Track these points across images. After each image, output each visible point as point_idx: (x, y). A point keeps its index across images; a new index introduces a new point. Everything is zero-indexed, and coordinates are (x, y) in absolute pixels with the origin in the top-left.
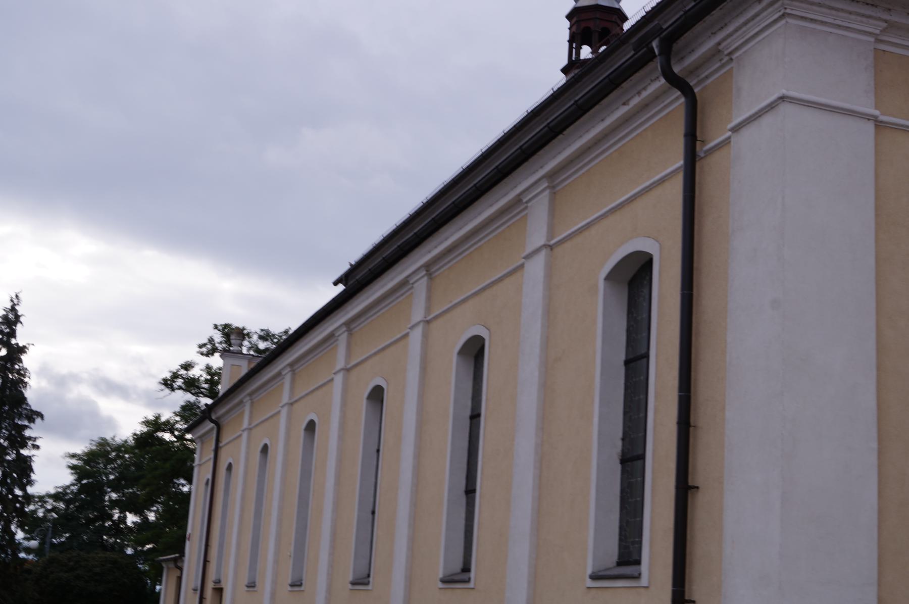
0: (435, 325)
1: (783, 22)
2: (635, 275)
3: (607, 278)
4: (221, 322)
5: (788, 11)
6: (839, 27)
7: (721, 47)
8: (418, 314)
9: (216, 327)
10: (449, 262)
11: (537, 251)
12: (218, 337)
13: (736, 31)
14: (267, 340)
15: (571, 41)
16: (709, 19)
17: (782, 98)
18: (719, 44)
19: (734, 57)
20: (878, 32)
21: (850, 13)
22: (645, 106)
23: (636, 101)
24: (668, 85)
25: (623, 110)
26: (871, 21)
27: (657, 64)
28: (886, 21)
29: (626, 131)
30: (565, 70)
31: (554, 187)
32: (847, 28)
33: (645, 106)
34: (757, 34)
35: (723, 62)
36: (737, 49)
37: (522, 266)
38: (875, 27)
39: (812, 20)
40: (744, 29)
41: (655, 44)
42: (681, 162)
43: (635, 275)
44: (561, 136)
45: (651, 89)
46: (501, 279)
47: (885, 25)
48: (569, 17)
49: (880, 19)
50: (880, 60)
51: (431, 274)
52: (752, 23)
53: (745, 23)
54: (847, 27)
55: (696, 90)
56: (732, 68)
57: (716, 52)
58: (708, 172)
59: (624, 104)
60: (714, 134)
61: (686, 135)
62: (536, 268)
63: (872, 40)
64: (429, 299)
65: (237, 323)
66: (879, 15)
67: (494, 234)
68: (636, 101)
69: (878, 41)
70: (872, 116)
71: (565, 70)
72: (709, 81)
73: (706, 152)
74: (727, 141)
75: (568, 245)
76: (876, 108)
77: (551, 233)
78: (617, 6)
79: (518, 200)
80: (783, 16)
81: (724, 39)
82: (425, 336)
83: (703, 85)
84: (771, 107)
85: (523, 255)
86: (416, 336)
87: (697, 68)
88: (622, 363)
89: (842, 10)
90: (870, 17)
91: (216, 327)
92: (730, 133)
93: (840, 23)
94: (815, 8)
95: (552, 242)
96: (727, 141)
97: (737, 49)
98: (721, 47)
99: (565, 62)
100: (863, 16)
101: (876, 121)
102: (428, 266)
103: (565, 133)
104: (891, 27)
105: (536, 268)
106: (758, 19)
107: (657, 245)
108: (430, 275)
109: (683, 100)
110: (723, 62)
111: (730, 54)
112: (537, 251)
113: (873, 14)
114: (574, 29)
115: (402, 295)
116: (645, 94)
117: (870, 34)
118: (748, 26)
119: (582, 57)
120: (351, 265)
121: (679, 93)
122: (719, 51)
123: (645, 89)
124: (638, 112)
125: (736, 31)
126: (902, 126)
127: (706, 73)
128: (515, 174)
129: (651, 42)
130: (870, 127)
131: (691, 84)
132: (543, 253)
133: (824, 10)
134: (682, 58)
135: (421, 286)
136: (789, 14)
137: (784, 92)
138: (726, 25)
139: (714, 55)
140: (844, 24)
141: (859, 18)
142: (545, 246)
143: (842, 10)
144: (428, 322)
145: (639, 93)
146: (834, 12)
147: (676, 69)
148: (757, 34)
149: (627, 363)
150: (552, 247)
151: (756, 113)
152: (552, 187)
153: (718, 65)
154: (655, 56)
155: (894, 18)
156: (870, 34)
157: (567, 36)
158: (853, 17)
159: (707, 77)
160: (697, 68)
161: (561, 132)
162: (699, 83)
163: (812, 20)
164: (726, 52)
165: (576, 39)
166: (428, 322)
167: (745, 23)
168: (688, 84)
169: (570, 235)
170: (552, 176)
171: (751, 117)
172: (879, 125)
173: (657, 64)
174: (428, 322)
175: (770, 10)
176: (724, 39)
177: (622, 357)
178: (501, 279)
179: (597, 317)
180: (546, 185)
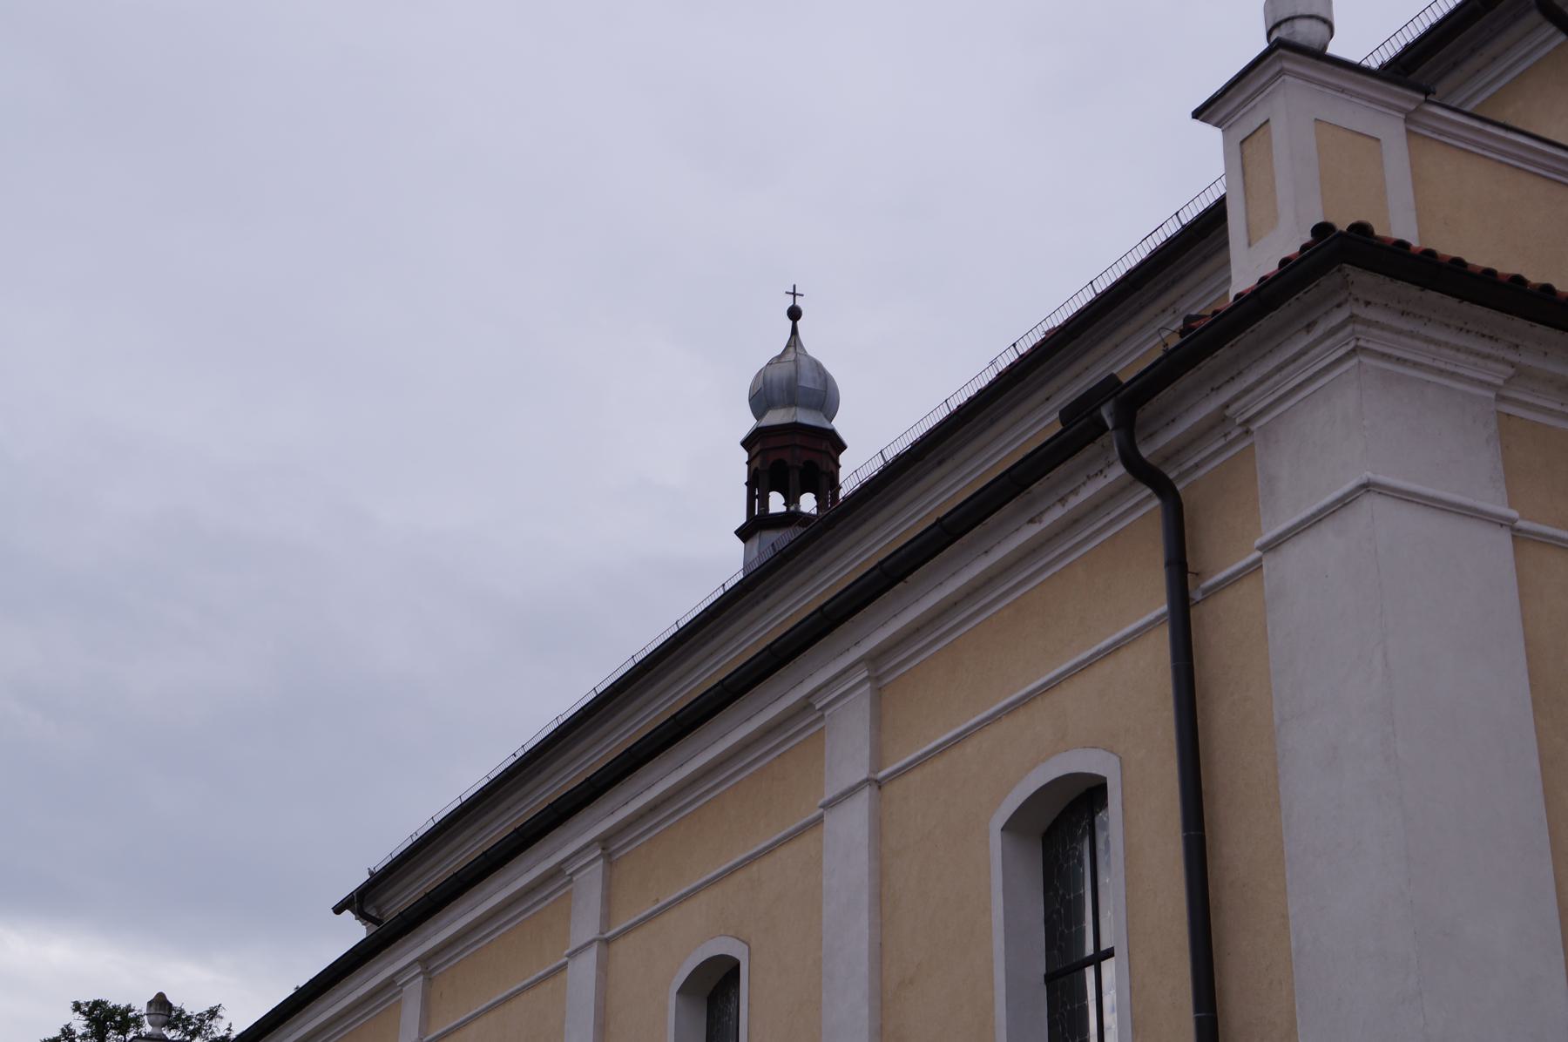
0: (620, 947)
1: (1353, 362)
2: (1064, 824)
3: (1006, 828)
4: (87, 997)
5: (1362, 343)
6: (1441, 372)
7: (1228, 412)
8: (585, 926)
9: (77, 1007)
10: (650, 829)
11: (852, 791)
12: (79, 1025)
13: (1260, 382)
14: (176, 1027)
15: (751, 484)
16: (1208, 364)
17: (1367, 487)
18: (1227, 406)
19: (1254, 427)
20: (1500, 382)
21: (1458, 350)
22: (1072, 523)
23: (1056, 514)
24: (1130, 477)
25: (1030, 532)
26: (1491, 364)
27: (1111, 440)
28: (1513, 365)
29: (1025, 574)
30: (744, 533)
31: (878, 679)
32: (1452, 375)
33: (1072, 523)
34: (1300, 386)
35: (1230, 437)
36: (1261, 413)
37: (819, 820)
38: (1496, 374)
39: (1399, 360)
40: (1277, 377)
41: (1105, 412)
42: (1164, 608)
43: (1064, 824)
44: (901, 584)
45: (1100, 484)
46: (769, 850)
47: (1511, 371)
48: (747, 444)
49: (1503, 361)
50: (1508, 431)
51: (610, 855)
52: (1291, 368)
53: (1280, 368)
54: (1453, 373)
55: (1179, 487)
56: (1252, 444)
57: (1220, 420)
58: (1218, 627)
59: (1032, 521)
60: (1219, 560)
61: (1168, 564)
62: (851, 826)
63: (1492, 395)
64: (608, 900)
65: (116, 999)
66: (1501, 353)
67: (746, 773)
68: (1056, 514)
69: (1501, 398)
70: (1508, 519)
71: (744, 533)
72: (1202, 472)
73: (1205, 591)
74: (1256, 566)
75: (915, 777)
76: (1511, 506)
77: (877, 759)
78: (827, 425)
79: (805, 705)
80: (1354, 351)
81: (1236, 398)
82: (603, 967)
83: (1189, 480)
84: (1344, 502)
85: (820, 802)
86: (584, 970)
87: (1178, 452)
88: (1042, 980)
89: (1446, 344)
90: (1488, 357)
91: (77, 1007)
92: (1258, 554)
93: (1442, 365)
94: (1403, 339)
95: (881, 774)
96: (1256, 566)
97: (1261, 413)
98: (1228, 412)
99: (741, 519)
100: (1478, 354)
101: (1512, 529)
102: (605, 841)
103: (909, 578)
104: (1520, 374)
105: (851, 826)
106: (1304, 359)
107: (1115, 759)
108: (608, 857)
109: (1156, 502)
110: (1230, 437)
111: (1248, 421)
112: (852, 791)
113: (1493, 352)
114: (757, 463)
115: (546, 898)
116: (1074, 502)
117: (1489, 385)
118: (1284, 372)
119: (772, 511)
120: (371, 873)
121: (1149, 491)
122: (1224, 419)
123: (1075, 492)
124: (1057, 535)
125: (1260, 382)
126: (1552, 537)
127: (1197, 459)
128: (800, 660)
129: (1098, 407)
130: (1504, 538)
131: (1171, 476)
132: (865, 794)
133: (1418, 343)
134: (1151, 435)
135: (589, 884)
136: (1364, 349)
137: (1367, 475)
138: (1240, 373)
139: (1212, 427)
140: (1448, 367)
141: (1472, 359)
142: (867, 780)
143: (1446, 344)
144: (608, 942)
145: (1063, 500)
146: (1433, 348)
147: (1145, 451)
148: (1300, 386)
149: (1050, 978)
150: (880, 784)
151: (1314, 516)
152: (875, 679)
153: (1222, 442)
154: (1106, 429)
155: (1525, 359)
156: (1489, 385)
157: (742, 474)
158: (1462, 356)
159: (1197, 466)
160: (1178, 452)
161: (902, 578)
162: (1182, 476)
163: (1399, 360)
164: (1238, 421)
165: (758, 485)
166: (608, 942)
167: (1280, 368)
168: (1165, 477)
169: (920, 758)
170: (875, 659)
171: (1303, 522)
172: (1520, 537)
173: (1111, 440)
174: (608, 942)
175: (1328, 343)
176: (1236, 398)
177: (1043, 970)
178: (769, 850)
179: (991, 895)
180: (866, 674)
